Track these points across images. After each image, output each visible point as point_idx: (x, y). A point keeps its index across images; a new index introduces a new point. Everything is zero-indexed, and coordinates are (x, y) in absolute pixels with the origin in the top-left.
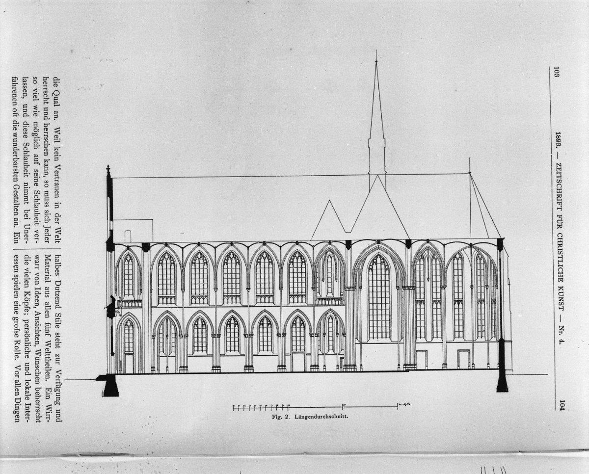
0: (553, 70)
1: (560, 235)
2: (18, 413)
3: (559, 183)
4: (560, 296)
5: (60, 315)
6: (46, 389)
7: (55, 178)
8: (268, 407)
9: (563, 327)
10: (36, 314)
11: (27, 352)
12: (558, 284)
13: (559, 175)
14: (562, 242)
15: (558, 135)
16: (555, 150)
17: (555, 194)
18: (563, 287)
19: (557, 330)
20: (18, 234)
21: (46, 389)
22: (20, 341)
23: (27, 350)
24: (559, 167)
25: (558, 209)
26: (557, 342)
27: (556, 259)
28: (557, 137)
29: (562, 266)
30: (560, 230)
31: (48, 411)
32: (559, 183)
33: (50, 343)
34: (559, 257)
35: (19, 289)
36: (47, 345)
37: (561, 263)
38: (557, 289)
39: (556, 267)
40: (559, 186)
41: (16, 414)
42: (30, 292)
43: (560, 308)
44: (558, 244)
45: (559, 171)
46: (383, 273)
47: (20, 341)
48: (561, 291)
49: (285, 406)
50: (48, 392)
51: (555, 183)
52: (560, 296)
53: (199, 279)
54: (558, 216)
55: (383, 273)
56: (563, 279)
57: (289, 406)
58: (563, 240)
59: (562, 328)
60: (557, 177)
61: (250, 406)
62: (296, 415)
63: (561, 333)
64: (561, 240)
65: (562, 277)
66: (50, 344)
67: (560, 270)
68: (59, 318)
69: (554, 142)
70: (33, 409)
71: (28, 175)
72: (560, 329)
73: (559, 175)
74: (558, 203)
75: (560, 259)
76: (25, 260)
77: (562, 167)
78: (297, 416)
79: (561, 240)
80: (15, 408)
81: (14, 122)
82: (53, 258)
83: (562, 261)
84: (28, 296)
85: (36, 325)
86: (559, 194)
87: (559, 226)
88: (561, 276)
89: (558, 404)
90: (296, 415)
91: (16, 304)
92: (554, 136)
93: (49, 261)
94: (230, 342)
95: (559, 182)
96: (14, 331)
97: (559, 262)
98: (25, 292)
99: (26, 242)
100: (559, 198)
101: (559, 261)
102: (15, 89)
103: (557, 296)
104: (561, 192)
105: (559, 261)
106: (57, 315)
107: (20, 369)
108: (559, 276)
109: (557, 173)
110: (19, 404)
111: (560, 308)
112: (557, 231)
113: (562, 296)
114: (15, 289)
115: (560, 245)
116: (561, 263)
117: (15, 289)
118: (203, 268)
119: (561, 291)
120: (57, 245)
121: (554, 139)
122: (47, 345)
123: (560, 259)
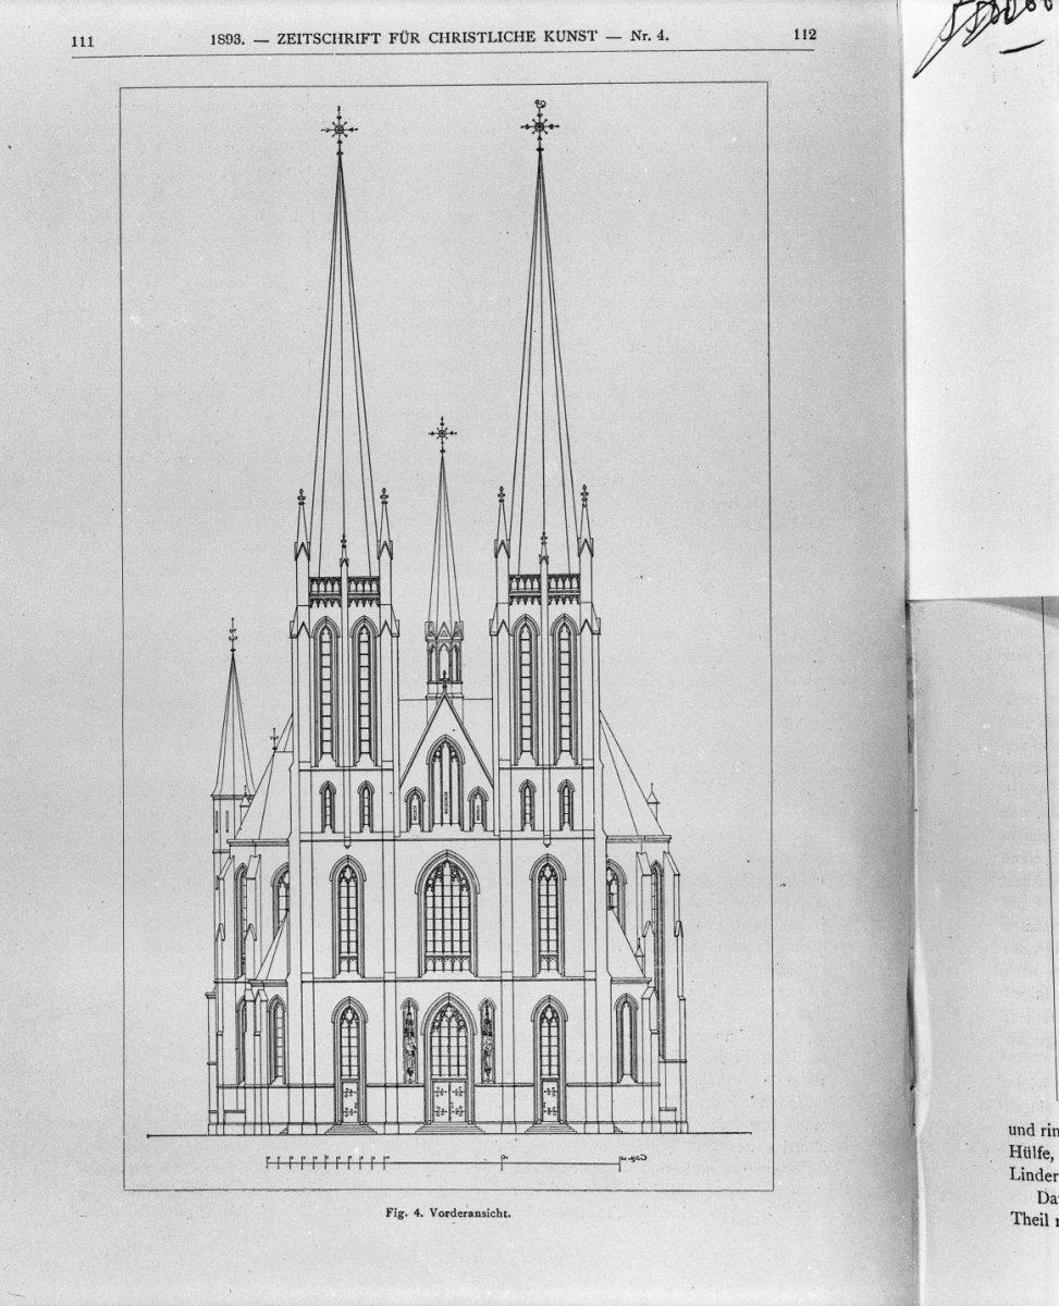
1: (434, 38)
3: (321, 37)
9: (634, 32)
12: (540, 44)
13: (303, 39)
14: (522, 32)
15: (217, 40)
16: (250, 47)
17: (451, 47)
18: (546, 32)
19: (639, 44)
24: (288, 38)
26: (663, 45)
27: (486, 46)
29: (500, 33)
30: (424, 37)
32: (321, 37)
34: (482, 41)
37: (495, 36)
38: (549, 46)
39: (504, 46)
40: (327, 38)
43: (592, 39)
44: (347, 42)
45: (296, 39)
48: (554, 36)
49: (379, 1159)
51: (322, 47)
53: (443, 930)
54: (392, 42)
56: (528, 32)
57: (387, 1160)
58: (338, 32)
59: (636, 35)
60: (308, 42)
64: (337, 36)
65: (525, 35)
67: (509, 37)
73: (303, 39)
74: (363, 42)
75: (486, 38)
77: (286, 32)
79: (337, 36)
83: (490, 33)
86: (451, 40)
87: (415, 38)
88: (341, 38)
89: (800, 44)
92: (218, 48)
94: (550, 1046)
95: (319, 39)
97: (493, 39)
100: (354, 39)
103: (565, 46)
104: (448, 34)
108: (341, 42)
109: (299, 43)
111: (592, 39)
112: (425, 45)
113: (567, 34)
115: (455, 39)
116: (495, 36)
118: (460, 896)
119: (554, 36)
121: (225, 48)
123: (486, 38)
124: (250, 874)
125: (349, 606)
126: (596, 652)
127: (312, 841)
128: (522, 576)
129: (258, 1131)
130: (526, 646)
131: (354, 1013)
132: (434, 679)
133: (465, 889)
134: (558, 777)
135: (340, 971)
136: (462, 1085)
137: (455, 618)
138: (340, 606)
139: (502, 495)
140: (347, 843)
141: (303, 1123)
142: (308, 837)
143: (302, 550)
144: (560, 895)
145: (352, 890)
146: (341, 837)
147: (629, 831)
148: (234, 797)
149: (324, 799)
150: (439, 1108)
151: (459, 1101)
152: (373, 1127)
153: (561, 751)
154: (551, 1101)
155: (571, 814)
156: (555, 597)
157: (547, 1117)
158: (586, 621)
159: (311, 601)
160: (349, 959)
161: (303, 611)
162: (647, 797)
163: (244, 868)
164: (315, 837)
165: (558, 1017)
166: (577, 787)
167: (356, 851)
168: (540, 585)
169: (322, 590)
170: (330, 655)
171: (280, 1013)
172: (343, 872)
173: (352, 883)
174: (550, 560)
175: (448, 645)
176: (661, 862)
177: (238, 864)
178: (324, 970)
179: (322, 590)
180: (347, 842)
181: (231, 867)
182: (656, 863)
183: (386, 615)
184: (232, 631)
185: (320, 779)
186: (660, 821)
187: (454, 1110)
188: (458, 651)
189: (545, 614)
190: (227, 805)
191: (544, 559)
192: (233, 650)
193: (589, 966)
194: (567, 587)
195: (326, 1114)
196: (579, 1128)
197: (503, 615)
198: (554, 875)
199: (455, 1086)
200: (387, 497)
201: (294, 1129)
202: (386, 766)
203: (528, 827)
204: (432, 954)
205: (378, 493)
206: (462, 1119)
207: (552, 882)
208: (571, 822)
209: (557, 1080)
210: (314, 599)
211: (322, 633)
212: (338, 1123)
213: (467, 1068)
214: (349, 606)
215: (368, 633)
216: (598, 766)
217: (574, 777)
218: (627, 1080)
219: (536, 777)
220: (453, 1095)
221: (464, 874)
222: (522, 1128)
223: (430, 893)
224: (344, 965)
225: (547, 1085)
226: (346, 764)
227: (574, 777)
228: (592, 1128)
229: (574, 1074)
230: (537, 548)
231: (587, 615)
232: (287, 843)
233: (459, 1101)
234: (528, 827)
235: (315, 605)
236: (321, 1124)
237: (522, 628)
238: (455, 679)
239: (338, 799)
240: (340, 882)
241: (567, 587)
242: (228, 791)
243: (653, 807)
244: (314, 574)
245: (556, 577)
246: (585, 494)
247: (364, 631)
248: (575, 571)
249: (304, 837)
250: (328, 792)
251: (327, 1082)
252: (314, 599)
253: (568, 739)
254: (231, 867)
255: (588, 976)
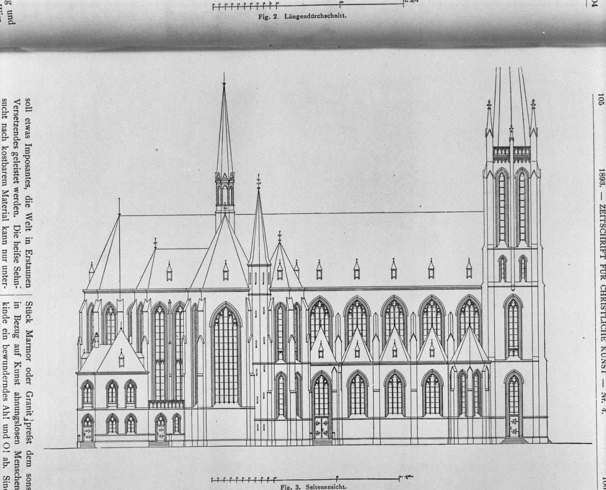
0: (597, 98)
2: (17, 155)
3: (603, 228)
4: (603, 358)
5: (31, 303)
6: (26, 251)
7: (26, 308)
8: (241, 5)
10: (4, 408)
11: (17, 479)
16: (599, 190)
20: (31, 252)
21: (26, 251)
22: (20, 317)
23: (17, 476)
25: (601, 257)
28: (601, 175)
31: (28, 220)
32: (603, 228)
33: (30, 215)
34: (602, 313)
35: (19, 162)
36: (27, 218)
41: (15, 156)
42: (20, 363)
46: (230, 328)
47: (20, 317)
50: (29, 255)
52: (603, 358)
55: (230, 328)
57: (278, 5)
60: (601, 220)
61: (220, 4)
62: (286, 15)
63: (603, 401)
66: (31, 217)
68: (30, 308)
69: (598, 181)
70: (22, 273)
71: (31, 413)
72: (603, 397)
74: (601, 250)
76: (15, 480)
78: (288, 16)
80: (14, 413)
81: (28, 198)
82: (23, 455)
84: (18, 367)
85: (15, 425)
90: (286, 15)
91: (16, 250)
93: (31, 338)
96: (13, 256)
98: (15, 363)
99: (20, 169)
101: (602, 317)
102: (4, 174)
105: (602, 317)
106: (28, 304)
107: (20, 104)
110: (19, 231)
114: (14, 162)
117: (14, 162)
120: (29, 291)
121: (598, 177)
122: (27, 218)
124: (200, 308)
125: (514, 162)
126: (539, 187)
127: (532, 286)
128: (500, 147)
129: (484, 442)
130: (502, 184)
131: (517, 378)
132: (220, 203)
133: (439, 314)
134: (519, 253)
135: (509, 356)
136: (517, 418)
137: (231, 171)
138: (509, 162)
139: (489, 105)
140: (513, 288)
141: (373, 439)
142: (492, 284)
143: (489, 132)
144: (520, 316)
145: (516, 313)
146: (509, 284)
147: (298, 285)
148: (259, 265)
149: (500, 265)
150: (317, 431)
151: (325, 428)
152: (526, 439)
153: (500, 240)
154: (514, 427)
155: (505, 273)
156: (517, 159)
157: (512, 435)
158: (534, 171)
159: (494, 159)
160: (514, 350)
161: (490, 165)
162: (294, 267)
163: (141, 305)
164: (496, 284)
165: (518, 381)
166: (509, 260)
167: (518, 292)
168: (509, 153)
169: (500, 154)
170: (524, 187)
171: (463, 378)
172: (511, 303)
173: (515, 309)
174: (515, 140)
175: (227, 185)
176: (143, 303)
177: (193, 303)
178: (501, 355)
179: (500, 154)
180: (513, 287)
181: (189, 305)
182: (297, 303)
183: (534, 167)
184: (258, 180)
185: (499, 254)
186: (300, 280)
187: (320, 434)
188: (232, 188)
189: (512, 167)
190: (256, 269)
191: (512, 139)
192: (259, 188)
193: (536, 354)
194: (523, 154)
195: (502, 433)
196: (530, 440)
197: (490, 167)
198: (516, 305)
199: (324, 420)
200: (488, 105)
201: (188, 444)
202: (534, 246)
203: (523, 280)
204: (512, 348)
205: (530, 102)
206: (517, 435)
207: (515, 309)
208: (505, 278)
209: (518, 416)
210: (496, 159)
211: (500, 176)
212: (508, 436)
213: (328, 410)
214: (514, 162)
215: (504, 176)
216: (540, 248)
217: (527, 253)
218: (281, 417)
219: (507, 254)
220: (323, 425)
221: (326, 307)
222: (499, 441)
223: (462, 315)
224: (511, 353)
225: (512, 418)
226: (513, 246)
227: (527, 253)
228: (536, 440)
229: (527, 412)
230: (508, 135)
231: (534, 167)
232: (481, 288)
233: (318, 428)
234: (523, 280)
235: (496, 162)
236: (499, 438)
237: (521, 174)
238: (230, 203)
239: (508, 264)
240: (509, 308)
241: (523, 154)
242: (256, 262)
243: (297, 272)
244: (496, 145)
245: (518, 148)
246: (533, 104)
247: (502, 175)
248: (528, 145)
249: (490, 284)
250: (523, 261)
251: (307, 418)
252: (496, 159)
253: (524, 234)
254: (189, 305)
255: (535, 359)
